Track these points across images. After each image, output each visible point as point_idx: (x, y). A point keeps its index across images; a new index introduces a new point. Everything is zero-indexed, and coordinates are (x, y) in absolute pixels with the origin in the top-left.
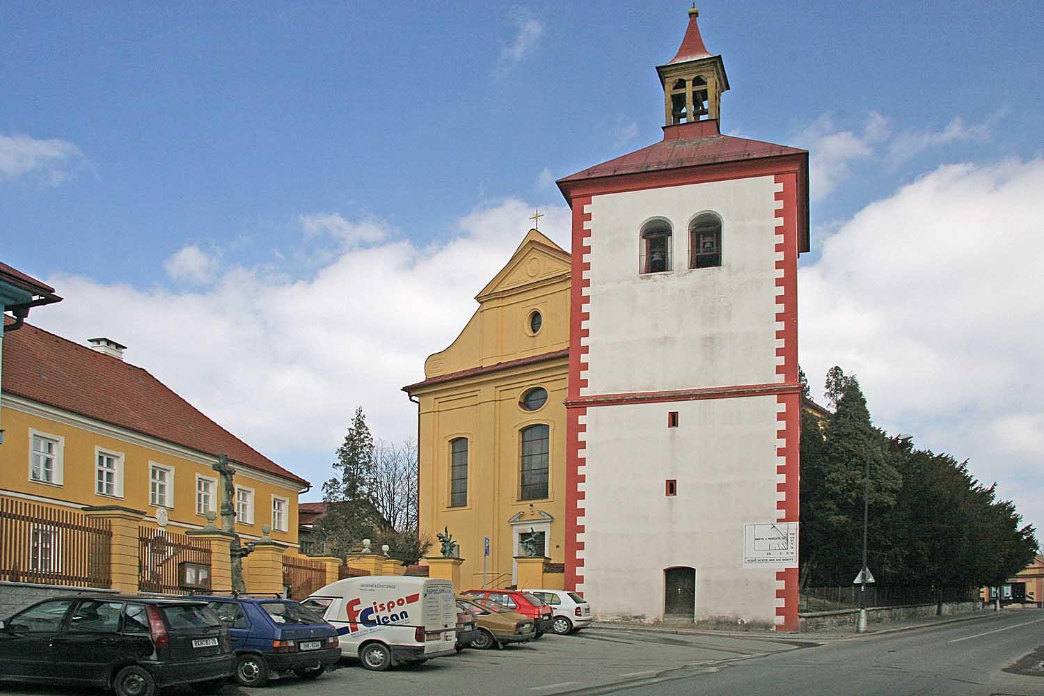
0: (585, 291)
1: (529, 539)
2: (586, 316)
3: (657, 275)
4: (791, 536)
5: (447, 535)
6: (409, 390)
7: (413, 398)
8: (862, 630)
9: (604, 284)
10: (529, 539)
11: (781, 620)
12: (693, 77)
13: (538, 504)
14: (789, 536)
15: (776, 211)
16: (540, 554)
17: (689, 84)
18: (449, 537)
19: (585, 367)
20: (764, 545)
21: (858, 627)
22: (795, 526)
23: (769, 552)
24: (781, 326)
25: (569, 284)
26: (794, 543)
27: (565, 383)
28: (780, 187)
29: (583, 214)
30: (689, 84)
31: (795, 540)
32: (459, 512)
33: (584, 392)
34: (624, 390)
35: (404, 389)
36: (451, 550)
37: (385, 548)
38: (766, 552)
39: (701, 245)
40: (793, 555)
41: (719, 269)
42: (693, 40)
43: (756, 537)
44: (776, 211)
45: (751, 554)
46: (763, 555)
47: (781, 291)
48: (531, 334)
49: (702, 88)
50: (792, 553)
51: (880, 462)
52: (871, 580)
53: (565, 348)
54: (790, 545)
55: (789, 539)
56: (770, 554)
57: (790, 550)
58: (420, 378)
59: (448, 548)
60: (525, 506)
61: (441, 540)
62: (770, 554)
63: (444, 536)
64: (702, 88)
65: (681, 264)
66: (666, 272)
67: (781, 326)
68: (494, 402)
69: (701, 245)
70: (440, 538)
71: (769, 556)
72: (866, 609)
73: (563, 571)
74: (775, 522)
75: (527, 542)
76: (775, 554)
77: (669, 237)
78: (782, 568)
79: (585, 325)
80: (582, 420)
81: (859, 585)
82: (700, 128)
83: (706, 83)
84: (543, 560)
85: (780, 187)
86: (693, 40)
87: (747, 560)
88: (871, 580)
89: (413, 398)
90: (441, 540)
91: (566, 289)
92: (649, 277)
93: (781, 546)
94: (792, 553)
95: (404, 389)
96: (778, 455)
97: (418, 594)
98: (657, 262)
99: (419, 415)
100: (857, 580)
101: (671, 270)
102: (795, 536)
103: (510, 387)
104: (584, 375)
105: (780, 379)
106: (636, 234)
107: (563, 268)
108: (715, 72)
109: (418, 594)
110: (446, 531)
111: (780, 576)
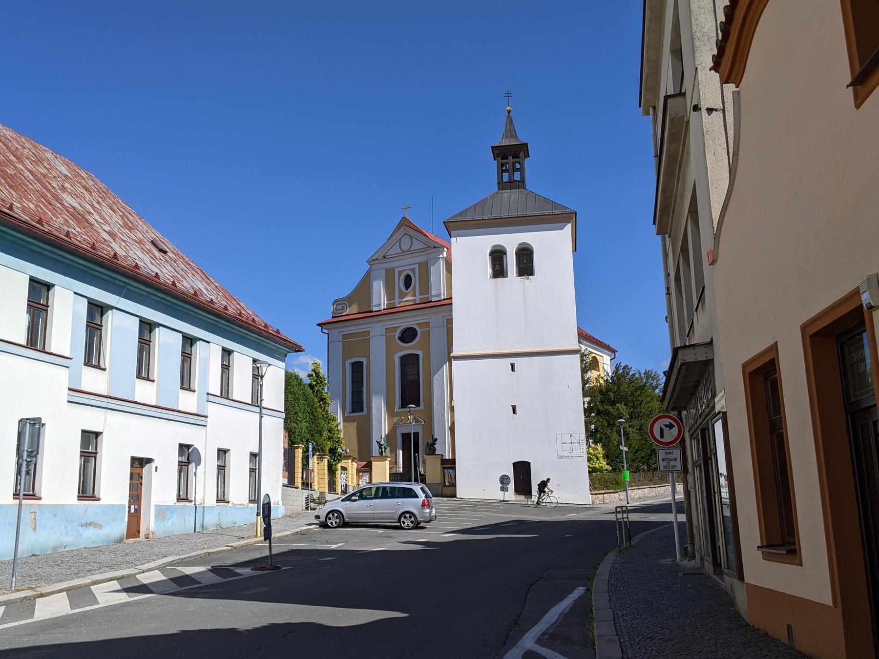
7: (324, 331)
14: (581, 441)
35: (319, 325)
38: (569, 451)
39: (522, 261)
40: (584, 454)
42: (511, 131)
43: (563, 442)
50: (583, 452)
51: (309, 409)
54: (581, 447)
55: (581, 443)
58: (328, 317)
69: (522, 261)
77: (504, 256)
82: (626, 493)
86: (511, 131)
89: (324, 331)
93: (577, 448)
94: (583, 452)
97: (774, 358)
98: (499, 271)
99: (328, 343)
109: (774, 358)
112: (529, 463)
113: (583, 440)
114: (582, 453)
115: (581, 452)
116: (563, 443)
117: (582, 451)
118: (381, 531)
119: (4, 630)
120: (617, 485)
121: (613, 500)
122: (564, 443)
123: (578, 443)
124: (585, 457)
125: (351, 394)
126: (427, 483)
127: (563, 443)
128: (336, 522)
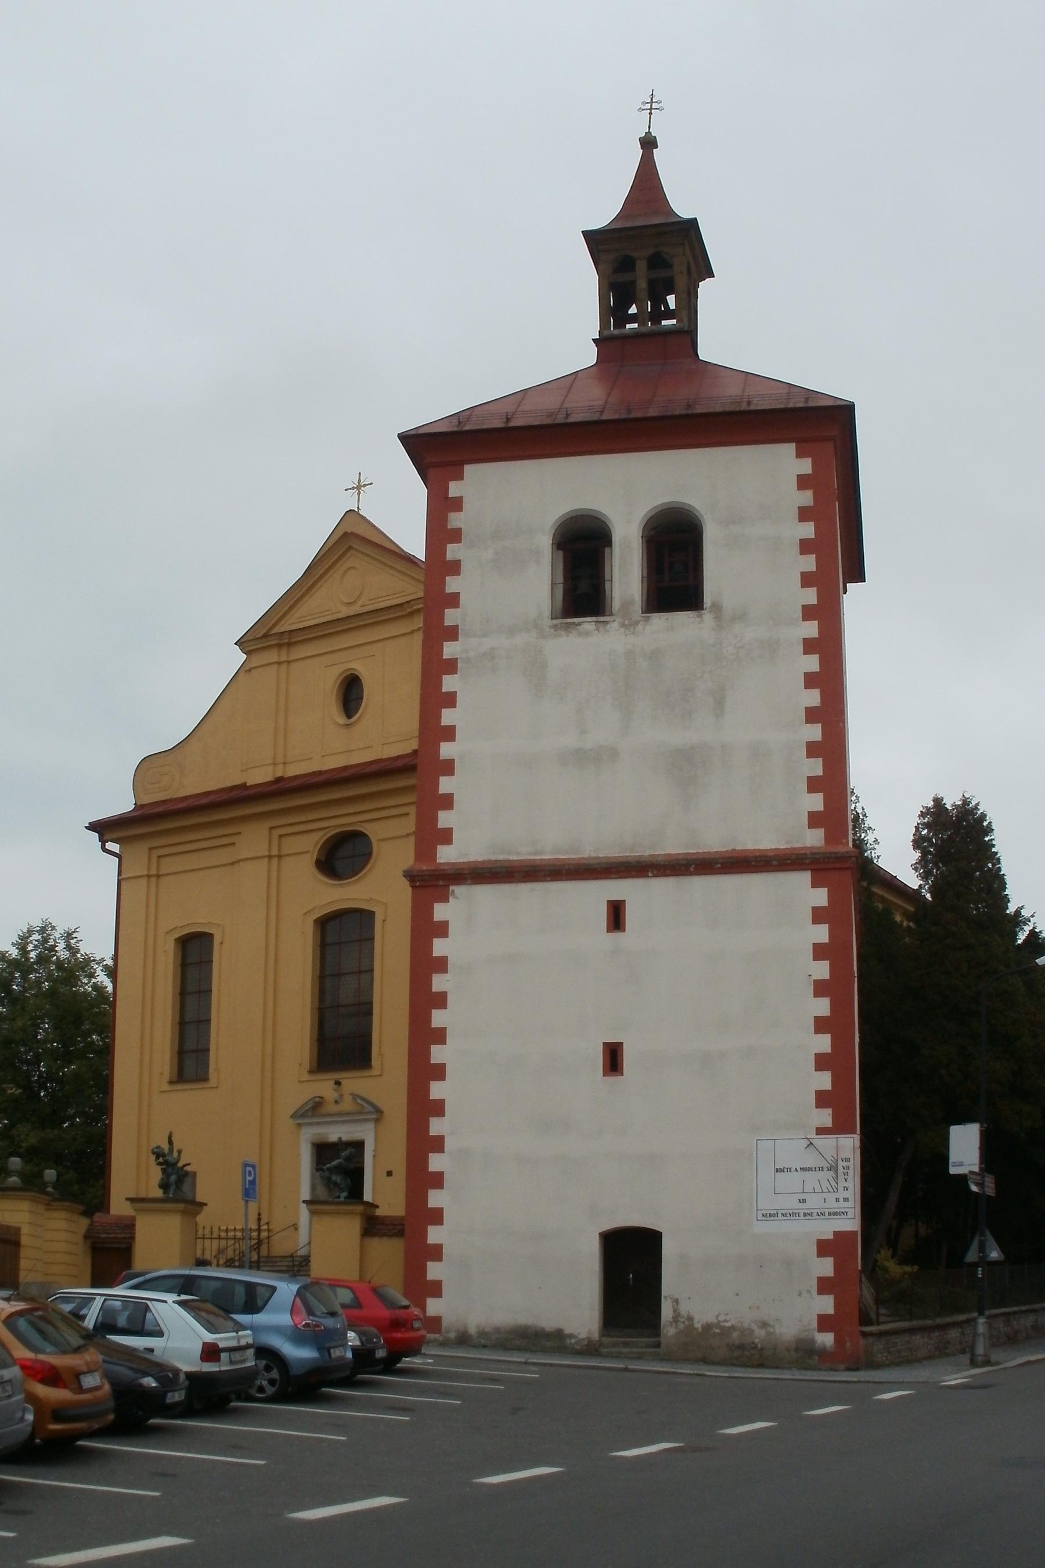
0: (449, 649)
1: (334, 1163)
2: (450, 700)
3: (588, 623)
4: (845, 1164)
5: (171, 1150)
6: (103, 828)
7: (110, 846)
8: (980, 1359)
9: (485, 635)
10: (334, 1163)
11: (827, 1339)
12: (651, 251)
13: (354, 1083)
14: (841, 1164)
15: (816, 946)
16: (356, 1192)
17: (641, 266)
18: (175, 1154)
19: (448, 802)
20: (790, 1182)
21: (973, 1355)
22: (850, 1145)
23: (802, 1197)
24: (815, 733)
25: (418, 622)
26: (850, 1177)
27: (409, 824)
28: (805, 466)
29: (447, 498)
30: (641, 266)
31: (851, 1172)
32: (190, 1097)
33: (446, 855)
34: (522, 853)
35: (93, 827)
36: (180, 1182)
37: (50, 1174)
40: (847, 1204)
41: (700, 616)
44: (816, 946)
45: (768, 1204)
46: (791, 1203)
47: (812, 664)
48: (342, 720)
49: (663, 274)
50: (846, 1200)
52: (995, 1254)
53: (410, 631)
54: (842, 1183)
55: (840, 1170)
56: (804, 1201)
57: (842, 1194)
58: (123, 803)
59: (173, 1178)
60: (324, 1087)
61: (161, 1160)
62: (804, 1201)
63: (166, 1151)
64: (663, 274)
65: (627, 605)
66: (602, 619)
67: (815, 733)
68: (275, 667)
70: (157, 1158)
71: (802, 1205)
72: (987, 1313)
73: (400, 1233)
74: (812, 1135)
75: (329, 1169)
76: (814, 1202)
78: (827, 1229)
79: (447, 716)
80: (440, 912)
81: (975, 1265)
83: (671, 266)
84: (360, 1208)
85: (805, 466)
87: (760, 1213)
88: (995, 1254)
90: (161, 1160)
91: (412, 632)
92: (567, 627)
94: (846, 1200)
95: (93, 827)
96: (808, 721)
100: (972, 1256)
101: (611, 614)
102: (851, 1164)
103: (302, 828)
104: (445, 820)
105: (814, 839)
106: (545, 542)
107: (411, 590)
108: (687, 248)
110: (170, 1142)
111: (824, 1248)
112: (661, 1233)
113: (848, 1160)
114: (842, 1204)
115: (837, 1200)
116: (777, 1171)
117: (842, 1194)
118: (954, 1380)
119: (300, 1507)
120: (250, 1287)
121: (277, 1386)
122: (782, 1170)
123: (829, 1169)
124: (850, 1215)
125: (178, 1027)
126: (24, 1277)
127: (777, 1171)
128: (272, 1382)
